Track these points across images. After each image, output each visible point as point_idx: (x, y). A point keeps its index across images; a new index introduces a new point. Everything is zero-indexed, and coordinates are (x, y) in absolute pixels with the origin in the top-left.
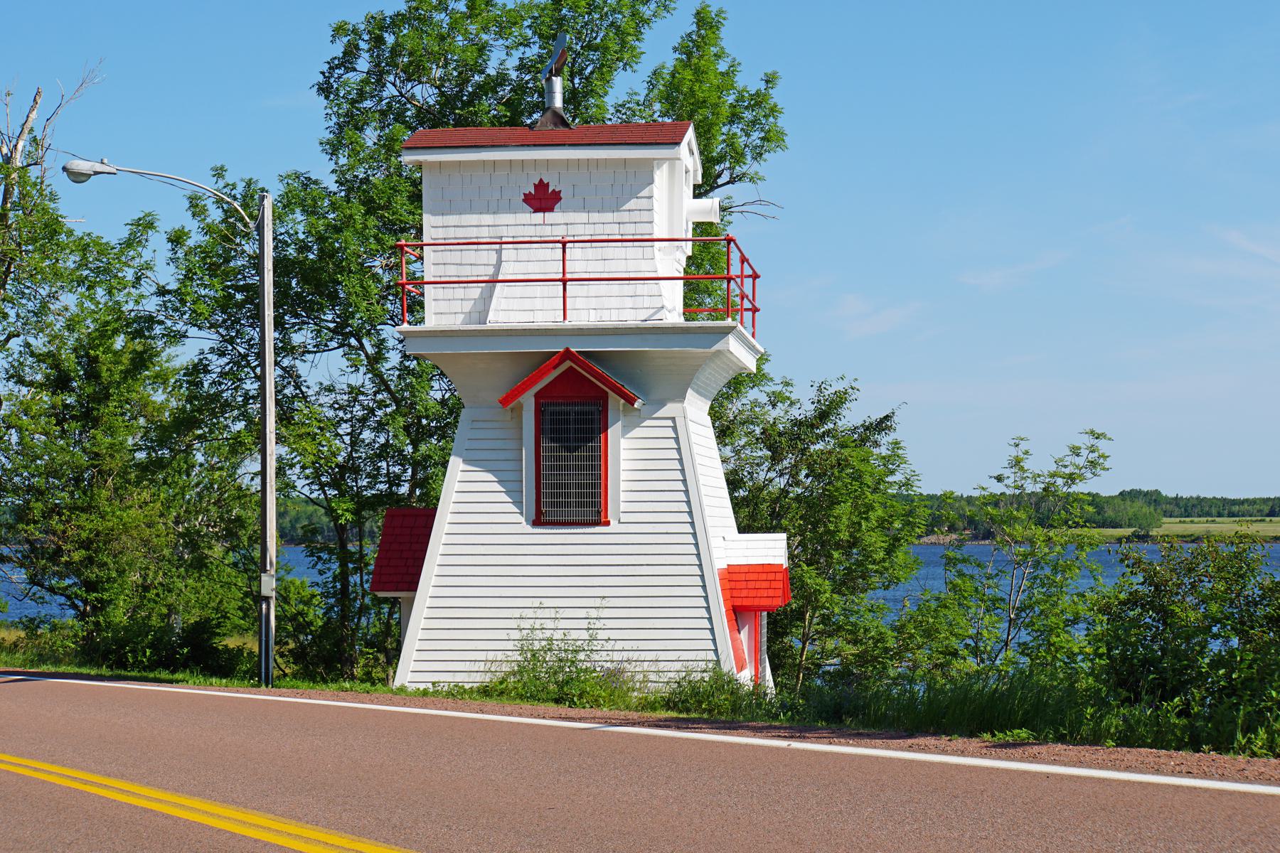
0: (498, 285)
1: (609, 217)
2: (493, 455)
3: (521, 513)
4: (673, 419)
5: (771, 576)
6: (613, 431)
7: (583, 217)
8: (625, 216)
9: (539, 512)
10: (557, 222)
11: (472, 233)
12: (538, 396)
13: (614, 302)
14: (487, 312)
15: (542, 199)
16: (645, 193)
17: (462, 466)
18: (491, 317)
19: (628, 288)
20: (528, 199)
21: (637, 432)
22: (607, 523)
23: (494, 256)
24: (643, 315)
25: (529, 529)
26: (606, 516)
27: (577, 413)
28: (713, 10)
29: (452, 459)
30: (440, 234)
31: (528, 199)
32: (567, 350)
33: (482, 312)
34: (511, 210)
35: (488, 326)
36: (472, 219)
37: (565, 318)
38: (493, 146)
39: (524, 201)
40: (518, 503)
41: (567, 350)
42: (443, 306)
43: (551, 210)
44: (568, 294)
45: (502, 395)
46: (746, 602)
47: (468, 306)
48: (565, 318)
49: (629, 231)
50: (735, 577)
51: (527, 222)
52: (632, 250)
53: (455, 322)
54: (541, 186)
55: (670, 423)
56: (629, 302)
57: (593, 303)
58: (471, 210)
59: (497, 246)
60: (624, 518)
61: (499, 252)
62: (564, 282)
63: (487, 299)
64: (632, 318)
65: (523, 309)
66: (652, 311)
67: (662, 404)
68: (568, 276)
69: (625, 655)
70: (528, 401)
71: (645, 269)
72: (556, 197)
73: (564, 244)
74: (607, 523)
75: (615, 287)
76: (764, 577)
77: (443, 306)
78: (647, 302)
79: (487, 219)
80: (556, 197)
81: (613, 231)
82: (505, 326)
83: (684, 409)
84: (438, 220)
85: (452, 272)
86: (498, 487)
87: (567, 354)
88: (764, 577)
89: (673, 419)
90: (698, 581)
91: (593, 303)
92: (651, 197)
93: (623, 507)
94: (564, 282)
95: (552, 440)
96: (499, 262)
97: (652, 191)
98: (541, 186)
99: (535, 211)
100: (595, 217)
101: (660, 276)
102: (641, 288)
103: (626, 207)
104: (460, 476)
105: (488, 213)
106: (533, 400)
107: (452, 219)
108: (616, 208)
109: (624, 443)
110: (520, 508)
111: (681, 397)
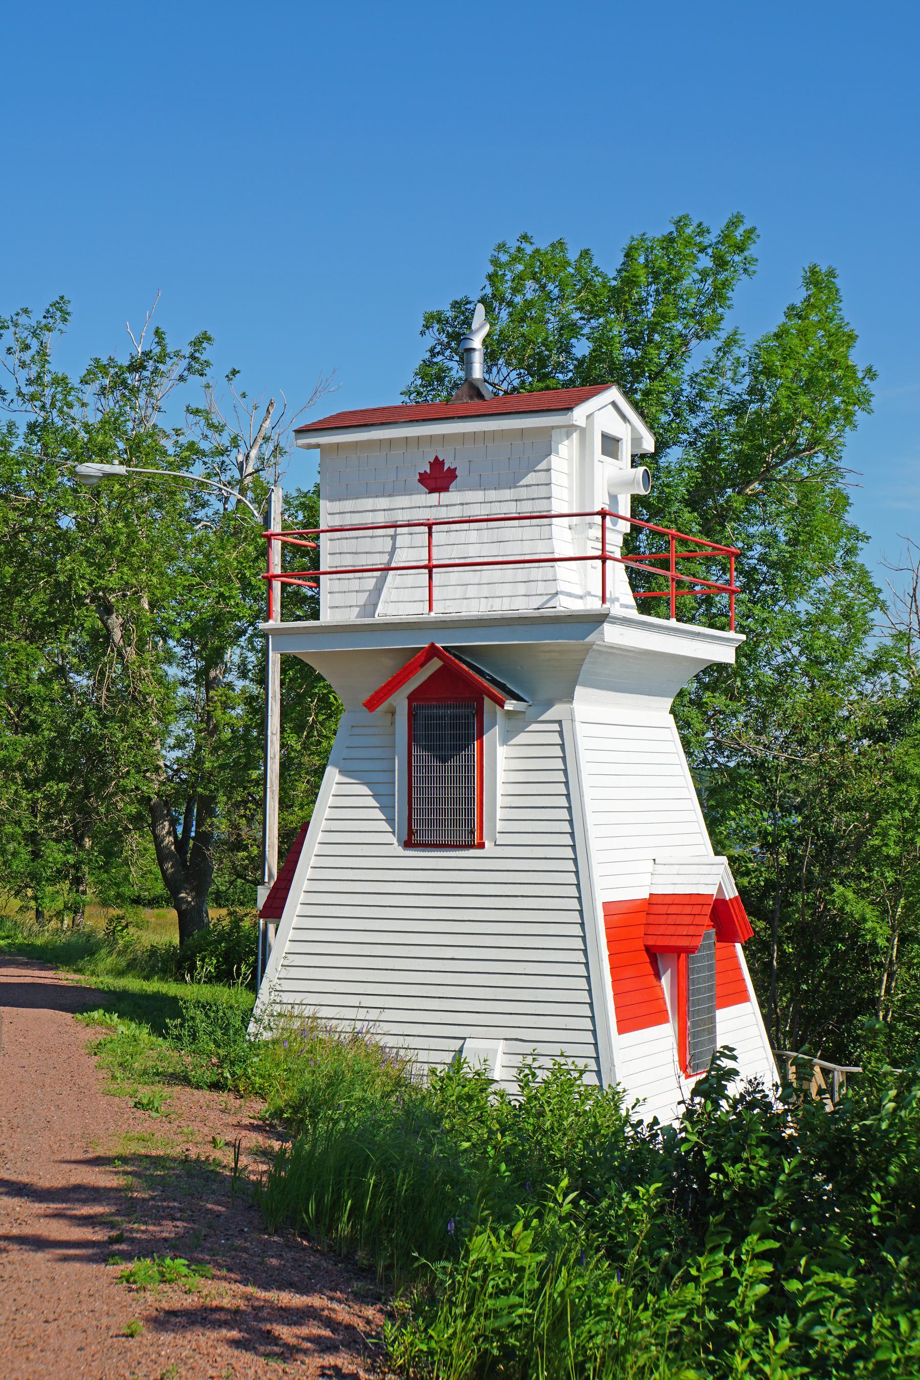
0: (391, 572)
1: (507, 494)
2: (365, 765)
3: (393, 833)
4: (560, 722)
5: (696, 910)
6: (493, 736)
7: (479, 495)
8: (523, 493)
9: (410, 832)
10: (454, 502)
11: (368, 519)
12: (411, 698)
13: (506, 590)
14: (375, 605)
15: (438, 479)
16: (543, 465)
17: (338, 778)
18: (380, 609)
19: (521, 572)
20: (424, 479)
21: (522, 738)
22: (481, 846)
23: (389, 542)
24: (536, 602)
25: (400, 851)
26: (481, 837)
27: (454, 717)
28: (823, 268)
29: (329, 769)
30: (336, 522)
31: (424, 479)
32: (432, 646)
33: (371, 606)
34: (407, 491)
35: (377, 619)
36: (368, 503)
37: (430, 609)
38: (382, 424)
39: (419, 481)
40: (390, 820)
41: (432, 646)
42: (339, 600)
43: (446, 489)
44: (434, 583)
45: (366, 696)
46: (661, 942)
47: (362, 598)
48: (430, 609)
49: (526, 508)
50: (656, 910)
51: (424, 504)
52: (528, 530)
53: (351, 617)
54: (437, 464)
55: (556, 727)
56: (522, 589)
57: (485, 591)
58: (368, 495)
59: (391, 531)
60: (501, 839)
61: (394, 537)
62: (430, 568)
63: (378, 590)
64: (524, 606)
65: (402, 601)
66: (546, 598)
67: (549, 705)
68: (435, 562)
69: (298, 998)
70: (400, 701)
71: (540, 550)
72: (452, 475)
73: (430, 526)
74: (481, 846)
75: (509, 572)
76: (688, 910)
77: (339, 600)
78: (541, 588)
79: (383, 503)
80: (452, 475)
81: (511, 509)
82: (396, 620)
83: (572, 712)
84: (337, 506)
85: (348, 561)
86: (372, 802)
87: (433, 651)
88: (688, 910)
89: (560, 722)
90: (576, 917)
91: (485, 591)
92: (549, 470)
93: (500, 826)
94: (430, 568)
95: (426, 748)
96: (394, 548)
97: (550, 462)
98: (437, 464)
99: (430, 492)
100: (492, 494)
101: (557, 556)
102: (536, 572)
103: (521, 483)
104: (334, 789)
105: (383, 496)
106: (406, 702)
107: (348, 505)
108: (513, 485)
109: (502, 751)
110: (393, 827)
111: (569, 697)
